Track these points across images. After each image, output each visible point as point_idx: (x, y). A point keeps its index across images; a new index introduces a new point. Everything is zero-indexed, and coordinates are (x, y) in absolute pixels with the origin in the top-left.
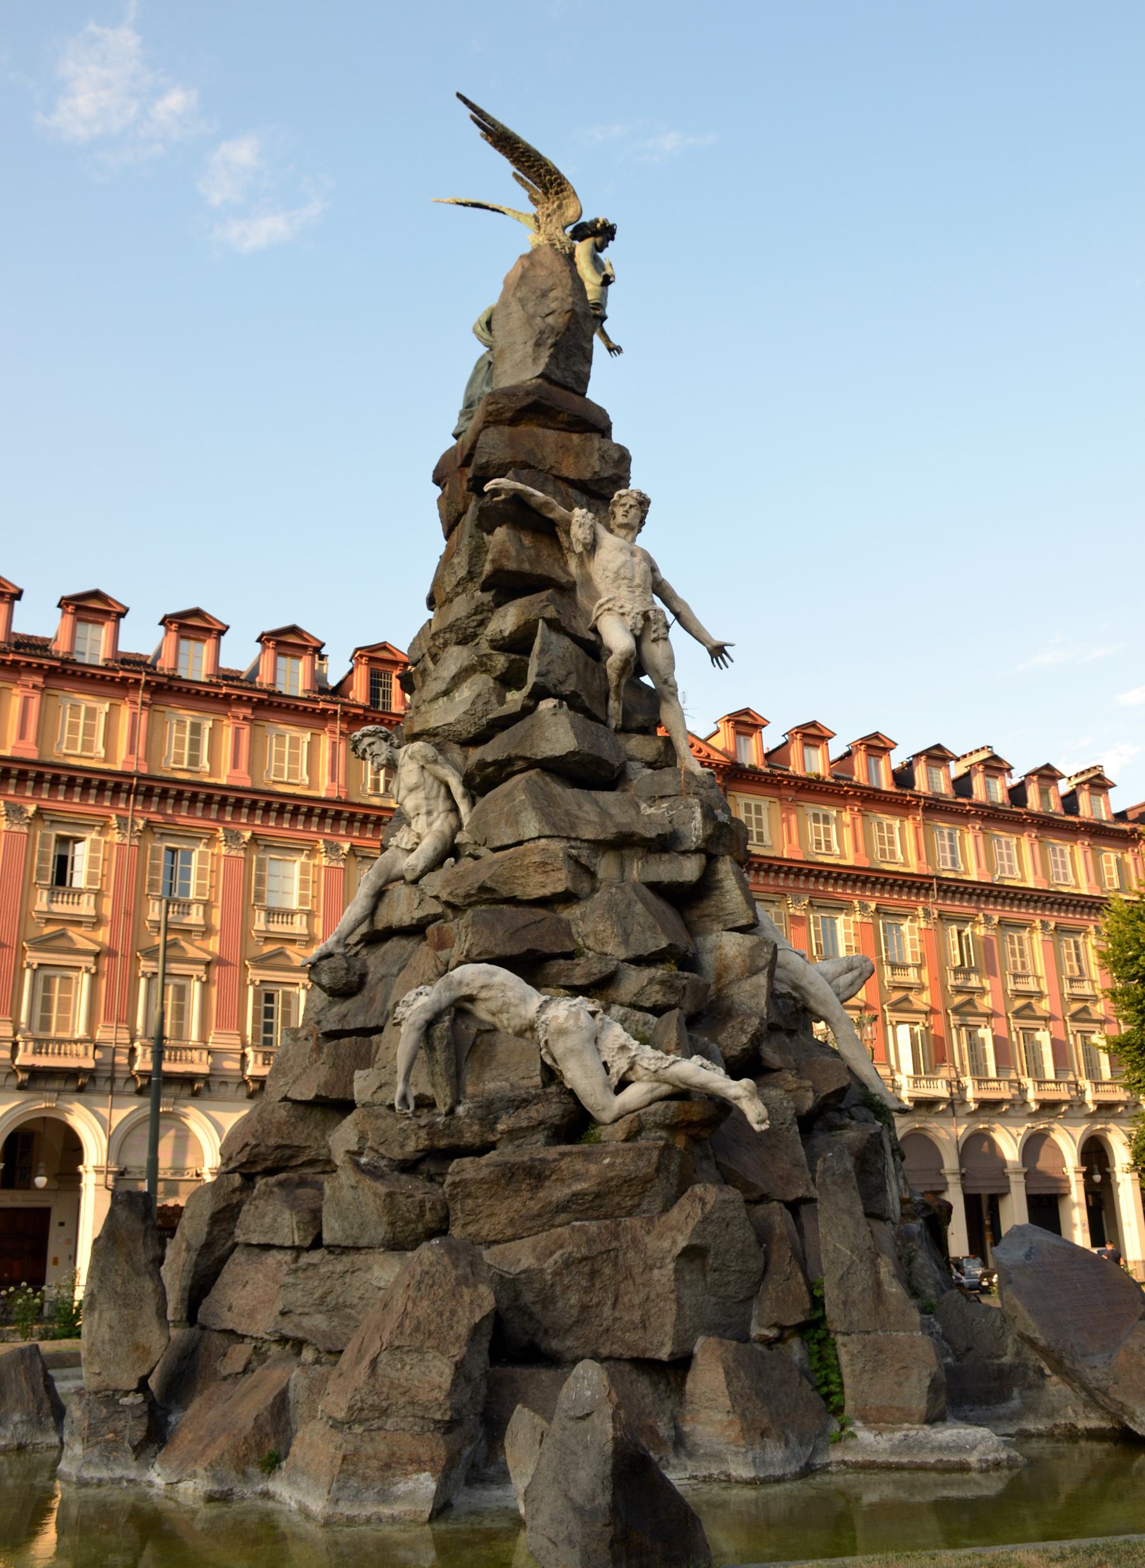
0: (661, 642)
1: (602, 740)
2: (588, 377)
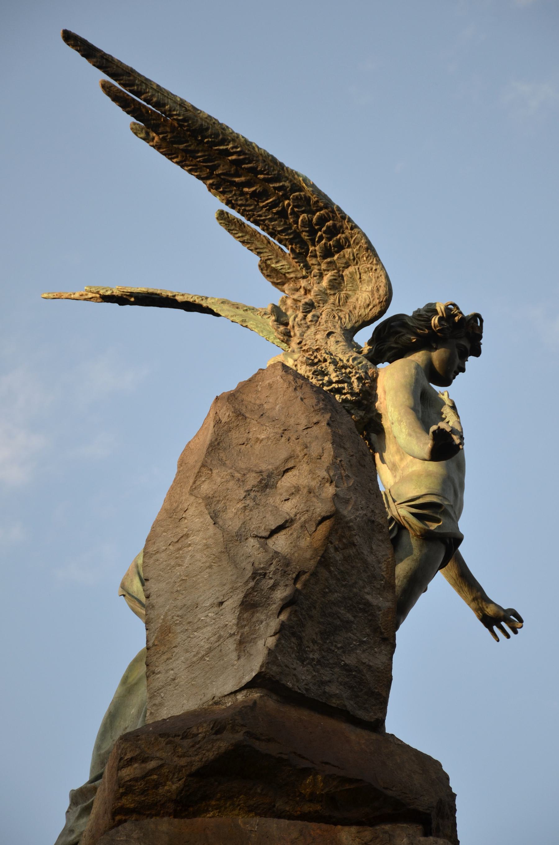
2: (385, 679)
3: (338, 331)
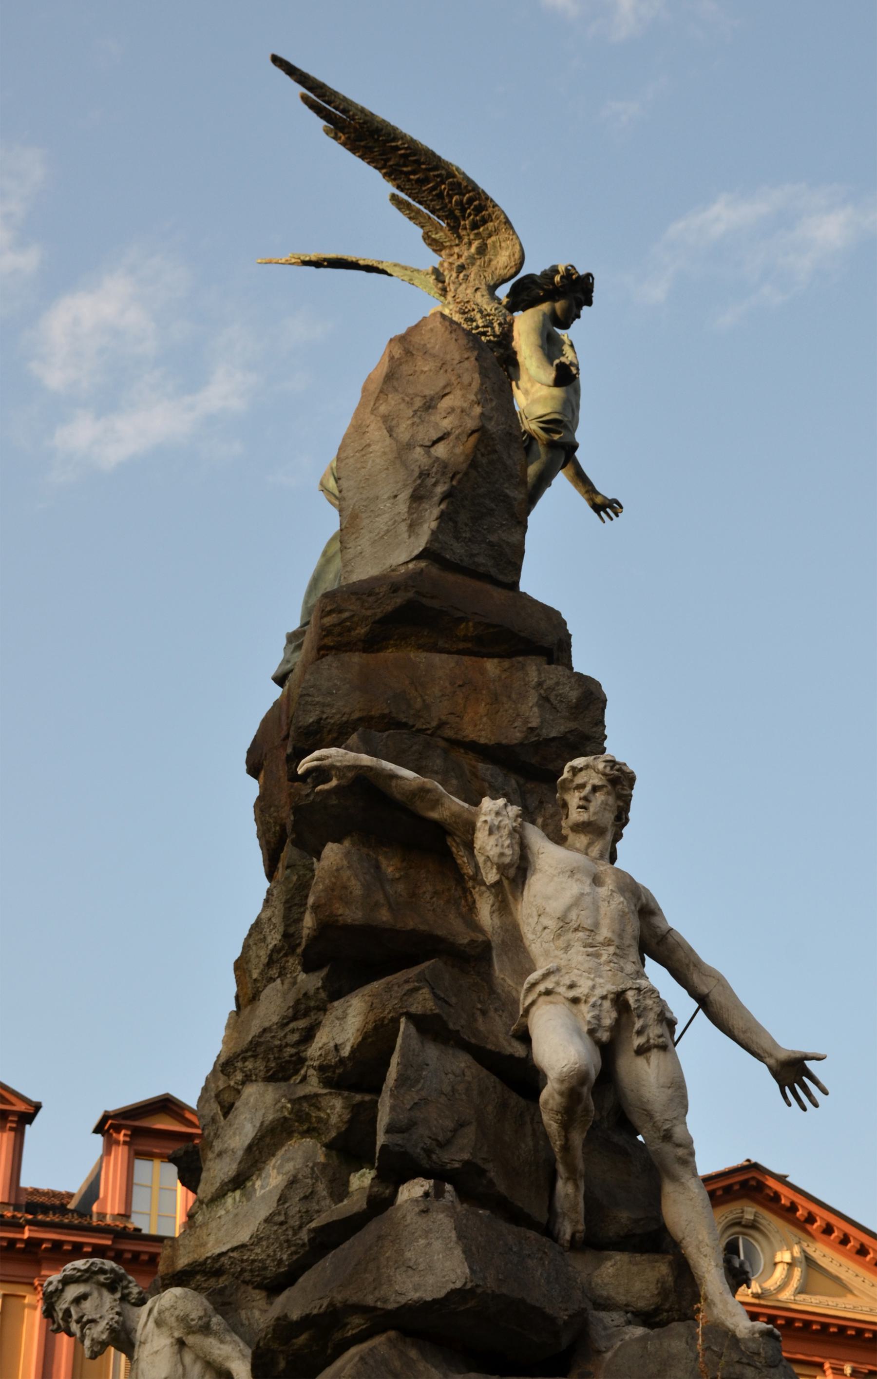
0: (655, 1056)
1: (531, 1263)
2: (520, 552)
3: (483, 287)
